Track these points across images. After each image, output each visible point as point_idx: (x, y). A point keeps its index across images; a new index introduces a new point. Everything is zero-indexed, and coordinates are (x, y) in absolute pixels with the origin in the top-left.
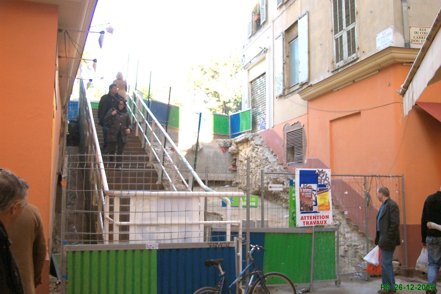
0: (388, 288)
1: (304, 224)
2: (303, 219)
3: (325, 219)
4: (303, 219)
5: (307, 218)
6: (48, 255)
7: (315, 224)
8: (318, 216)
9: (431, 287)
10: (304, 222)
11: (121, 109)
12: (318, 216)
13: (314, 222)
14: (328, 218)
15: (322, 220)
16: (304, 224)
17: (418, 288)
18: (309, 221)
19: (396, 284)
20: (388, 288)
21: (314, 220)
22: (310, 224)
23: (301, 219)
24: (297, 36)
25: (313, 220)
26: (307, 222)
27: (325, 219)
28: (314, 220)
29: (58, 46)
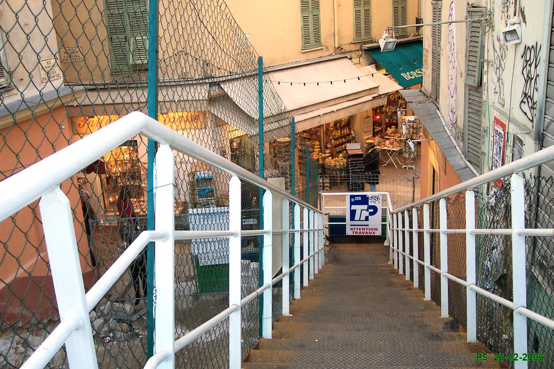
0: (485, 358)
1: (353, 233)
2: (352, 230)
3: (374, 231)
4: (352, 230)
5: (356, 229)
6: (390, 220)
7: (363, 234)
8: (367, 229)
9: (540, 357)
10: (353, 232)
11: (112, 336)
12: (367, 229)
13: (362, 232)
14: (377, 230)
15: (370, 231)
16: (353, 233)
17: (523, 358)
18: (366, 231)
19: (515, 353)
20: (485, 358)
21: (363, 231)
22: (359, 233)
23: (351, 230)
24: (89, 314)
25: (370, 231)
26: (356, 232)
27: (374, 231)
28: (363, 231)
29: (153, 323)
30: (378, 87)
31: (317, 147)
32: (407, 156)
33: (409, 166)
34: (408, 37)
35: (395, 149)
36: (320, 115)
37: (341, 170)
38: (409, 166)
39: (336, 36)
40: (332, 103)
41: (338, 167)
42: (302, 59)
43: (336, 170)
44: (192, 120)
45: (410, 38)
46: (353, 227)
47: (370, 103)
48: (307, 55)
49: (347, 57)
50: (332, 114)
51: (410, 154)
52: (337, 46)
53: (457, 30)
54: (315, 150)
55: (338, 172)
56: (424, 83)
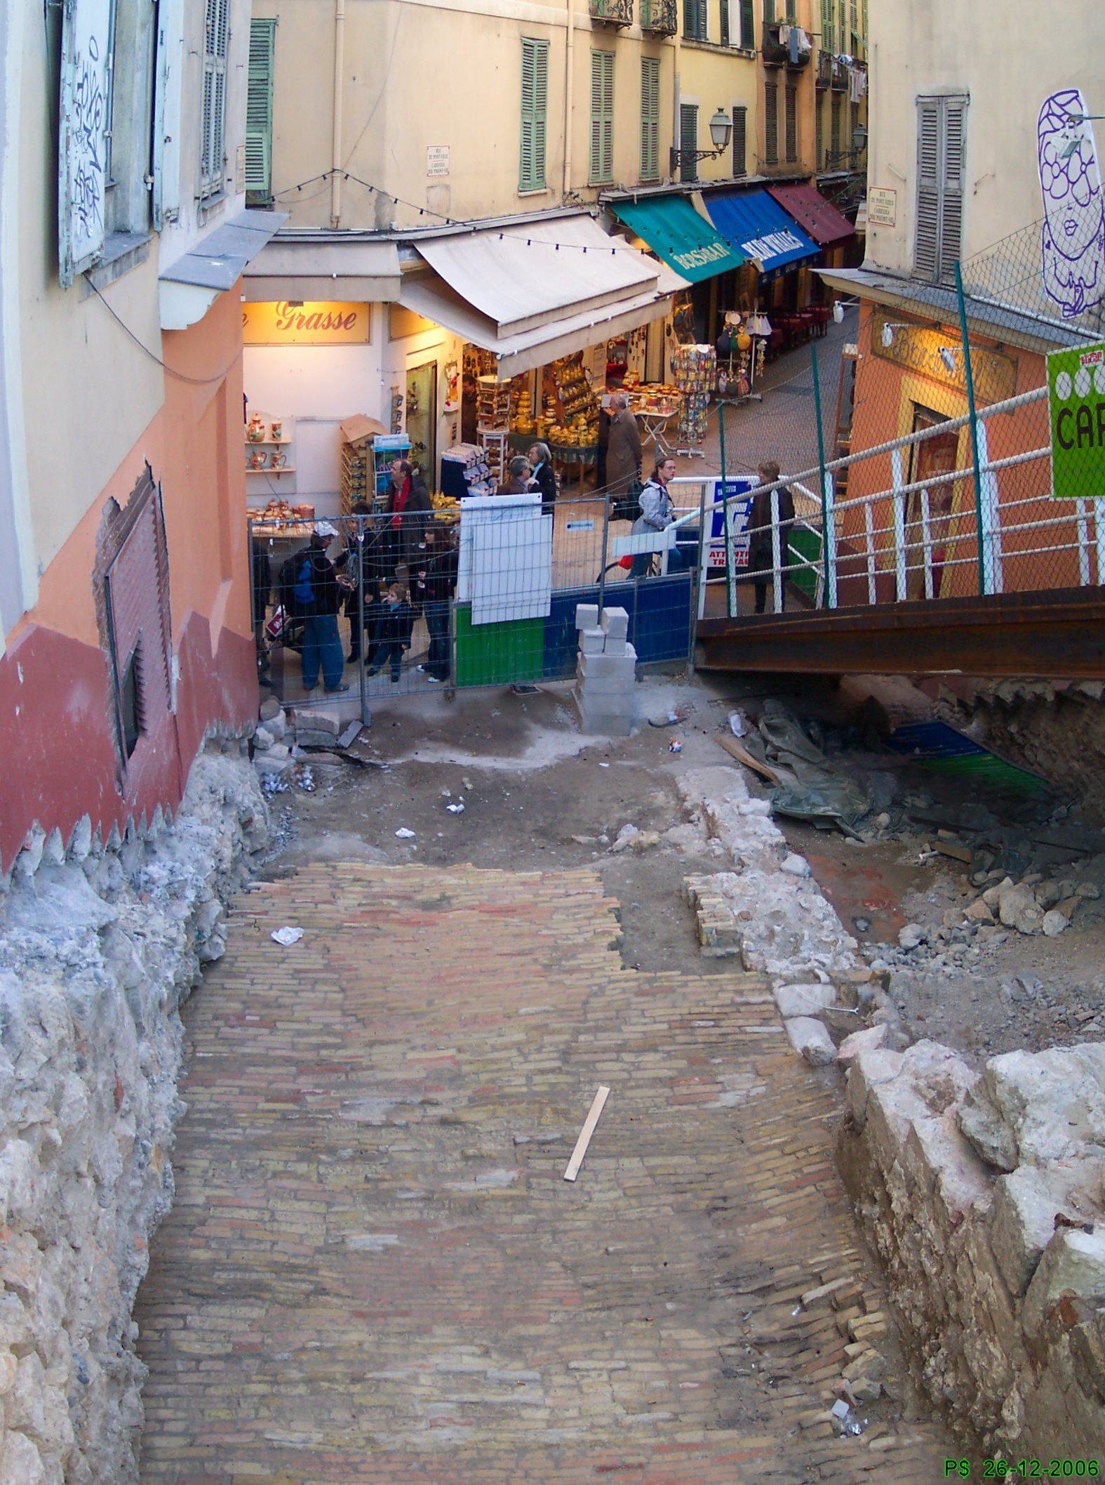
30: (655, 278)
31: (526, 403)
32: (690, 429)
33: (692, 451)
34: (659, 185)
35: (664, 415)
36: (605, 321)
37: (588, 451)
38: (692, 451)
39: (568, 170)
40: (597, 303)
41: (582, 445)
42: (517, 211)
43: (578, 452)
44: (339, 324)
45: (665, 188)
46: (715, 550)
47: (649, 311)
48: (525, 201)
49: (589, 214)
50: (604, 326)
51: (695, 425)
52: (567, 190)
53: (1097, 136)
54: (520, 410)
55: (582, 457)
56: (873, 253)
